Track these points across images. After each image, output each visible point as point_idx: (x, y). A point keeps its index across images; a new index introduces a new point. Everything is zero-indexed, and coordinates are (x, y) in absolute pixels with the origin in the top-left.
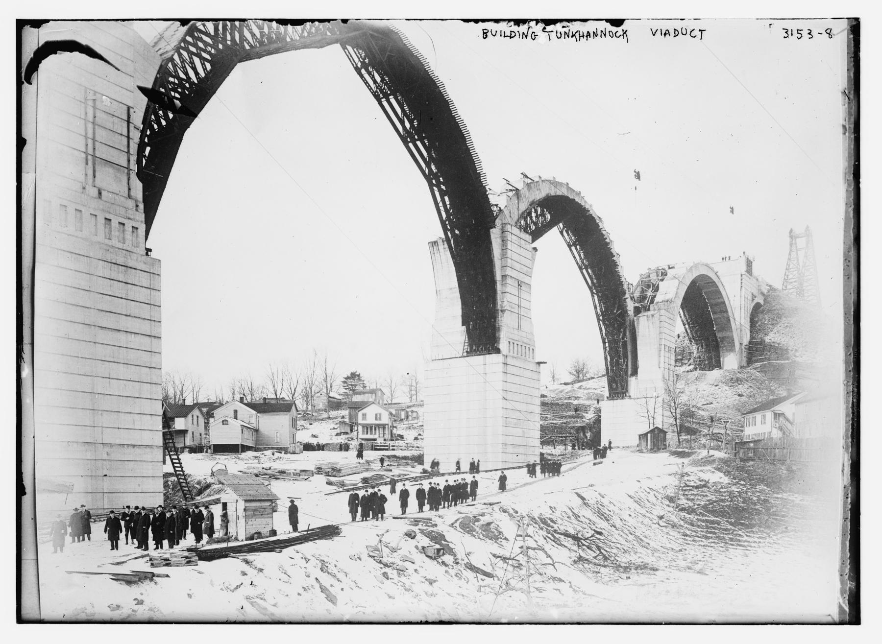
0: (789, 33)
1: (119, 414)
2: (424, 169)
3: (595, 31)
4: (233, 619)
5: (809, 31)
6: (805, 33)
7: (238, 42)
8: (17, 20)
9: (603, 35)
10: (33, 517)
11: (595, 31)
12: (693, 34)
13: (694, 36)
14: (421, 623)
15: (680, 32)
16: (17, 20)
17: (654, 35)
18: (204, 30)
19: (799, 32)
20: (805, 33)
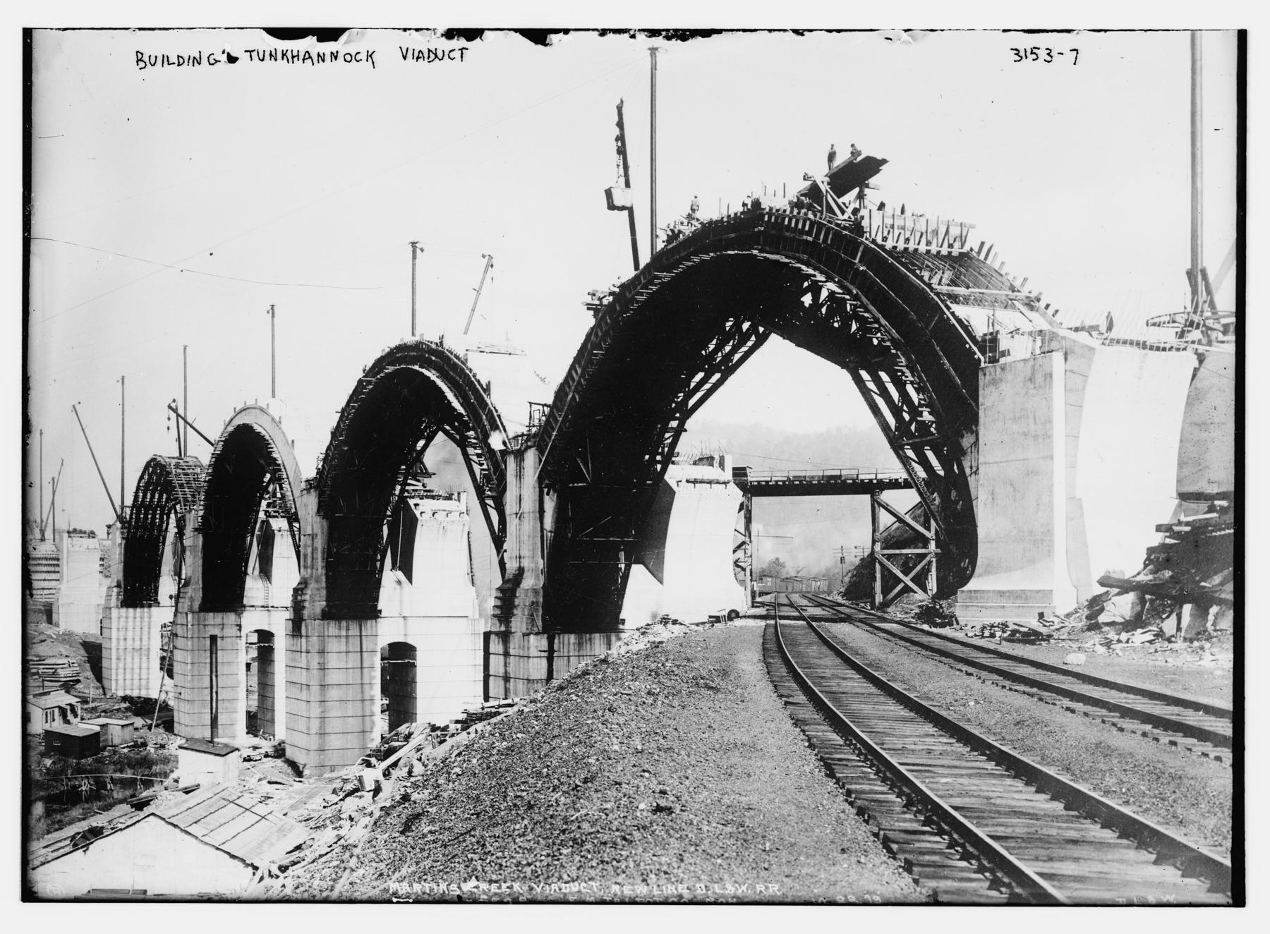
0: (1022, 54)
1: (293, 732)
2: (703, 389)
3: (198, 57)
4: (245, 895)
5: (1048, 51)
6: (1043, 54)
7: (744, 331)
8: (1246, 30)
9: (273, 53)
10: (150, 893)
11: (198, 57)
12: (358, 58)
13: (452, 57)
14: (775, 30)
15: (148, 63)
16: (1246, 30)
17: (178, 56)
18: (356, 794)
19: (1035, 51)
20: (1043, 54)
